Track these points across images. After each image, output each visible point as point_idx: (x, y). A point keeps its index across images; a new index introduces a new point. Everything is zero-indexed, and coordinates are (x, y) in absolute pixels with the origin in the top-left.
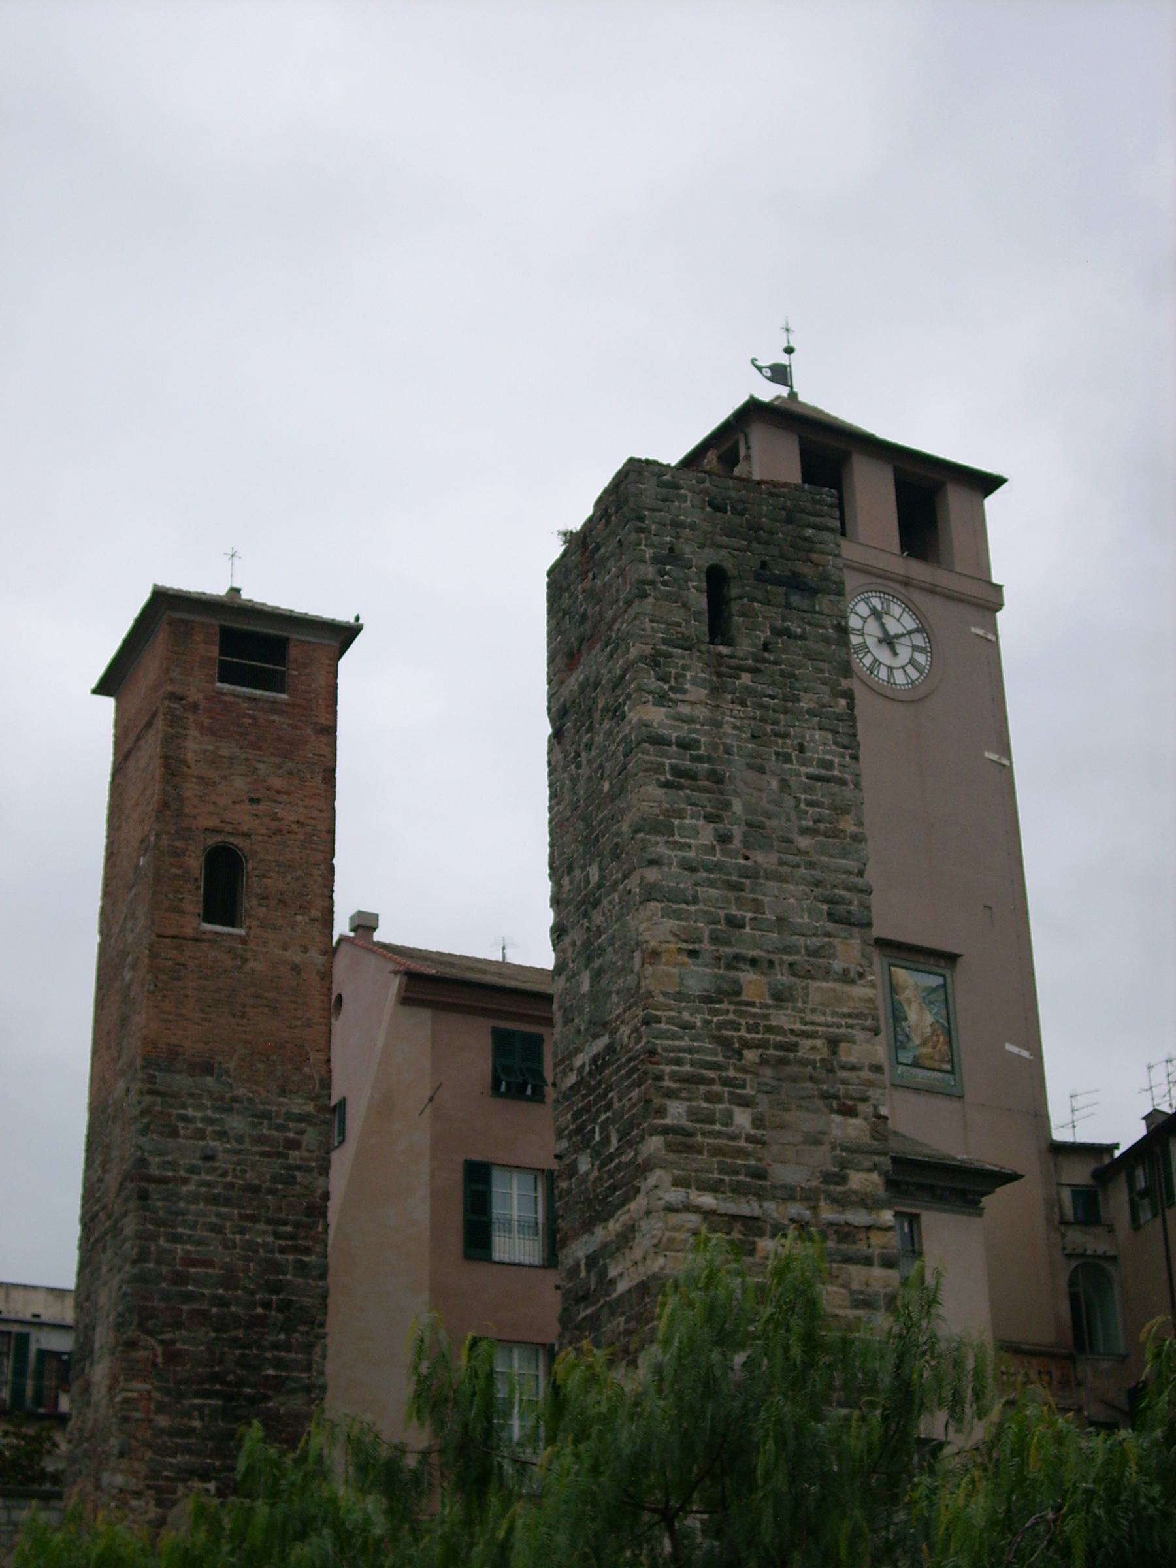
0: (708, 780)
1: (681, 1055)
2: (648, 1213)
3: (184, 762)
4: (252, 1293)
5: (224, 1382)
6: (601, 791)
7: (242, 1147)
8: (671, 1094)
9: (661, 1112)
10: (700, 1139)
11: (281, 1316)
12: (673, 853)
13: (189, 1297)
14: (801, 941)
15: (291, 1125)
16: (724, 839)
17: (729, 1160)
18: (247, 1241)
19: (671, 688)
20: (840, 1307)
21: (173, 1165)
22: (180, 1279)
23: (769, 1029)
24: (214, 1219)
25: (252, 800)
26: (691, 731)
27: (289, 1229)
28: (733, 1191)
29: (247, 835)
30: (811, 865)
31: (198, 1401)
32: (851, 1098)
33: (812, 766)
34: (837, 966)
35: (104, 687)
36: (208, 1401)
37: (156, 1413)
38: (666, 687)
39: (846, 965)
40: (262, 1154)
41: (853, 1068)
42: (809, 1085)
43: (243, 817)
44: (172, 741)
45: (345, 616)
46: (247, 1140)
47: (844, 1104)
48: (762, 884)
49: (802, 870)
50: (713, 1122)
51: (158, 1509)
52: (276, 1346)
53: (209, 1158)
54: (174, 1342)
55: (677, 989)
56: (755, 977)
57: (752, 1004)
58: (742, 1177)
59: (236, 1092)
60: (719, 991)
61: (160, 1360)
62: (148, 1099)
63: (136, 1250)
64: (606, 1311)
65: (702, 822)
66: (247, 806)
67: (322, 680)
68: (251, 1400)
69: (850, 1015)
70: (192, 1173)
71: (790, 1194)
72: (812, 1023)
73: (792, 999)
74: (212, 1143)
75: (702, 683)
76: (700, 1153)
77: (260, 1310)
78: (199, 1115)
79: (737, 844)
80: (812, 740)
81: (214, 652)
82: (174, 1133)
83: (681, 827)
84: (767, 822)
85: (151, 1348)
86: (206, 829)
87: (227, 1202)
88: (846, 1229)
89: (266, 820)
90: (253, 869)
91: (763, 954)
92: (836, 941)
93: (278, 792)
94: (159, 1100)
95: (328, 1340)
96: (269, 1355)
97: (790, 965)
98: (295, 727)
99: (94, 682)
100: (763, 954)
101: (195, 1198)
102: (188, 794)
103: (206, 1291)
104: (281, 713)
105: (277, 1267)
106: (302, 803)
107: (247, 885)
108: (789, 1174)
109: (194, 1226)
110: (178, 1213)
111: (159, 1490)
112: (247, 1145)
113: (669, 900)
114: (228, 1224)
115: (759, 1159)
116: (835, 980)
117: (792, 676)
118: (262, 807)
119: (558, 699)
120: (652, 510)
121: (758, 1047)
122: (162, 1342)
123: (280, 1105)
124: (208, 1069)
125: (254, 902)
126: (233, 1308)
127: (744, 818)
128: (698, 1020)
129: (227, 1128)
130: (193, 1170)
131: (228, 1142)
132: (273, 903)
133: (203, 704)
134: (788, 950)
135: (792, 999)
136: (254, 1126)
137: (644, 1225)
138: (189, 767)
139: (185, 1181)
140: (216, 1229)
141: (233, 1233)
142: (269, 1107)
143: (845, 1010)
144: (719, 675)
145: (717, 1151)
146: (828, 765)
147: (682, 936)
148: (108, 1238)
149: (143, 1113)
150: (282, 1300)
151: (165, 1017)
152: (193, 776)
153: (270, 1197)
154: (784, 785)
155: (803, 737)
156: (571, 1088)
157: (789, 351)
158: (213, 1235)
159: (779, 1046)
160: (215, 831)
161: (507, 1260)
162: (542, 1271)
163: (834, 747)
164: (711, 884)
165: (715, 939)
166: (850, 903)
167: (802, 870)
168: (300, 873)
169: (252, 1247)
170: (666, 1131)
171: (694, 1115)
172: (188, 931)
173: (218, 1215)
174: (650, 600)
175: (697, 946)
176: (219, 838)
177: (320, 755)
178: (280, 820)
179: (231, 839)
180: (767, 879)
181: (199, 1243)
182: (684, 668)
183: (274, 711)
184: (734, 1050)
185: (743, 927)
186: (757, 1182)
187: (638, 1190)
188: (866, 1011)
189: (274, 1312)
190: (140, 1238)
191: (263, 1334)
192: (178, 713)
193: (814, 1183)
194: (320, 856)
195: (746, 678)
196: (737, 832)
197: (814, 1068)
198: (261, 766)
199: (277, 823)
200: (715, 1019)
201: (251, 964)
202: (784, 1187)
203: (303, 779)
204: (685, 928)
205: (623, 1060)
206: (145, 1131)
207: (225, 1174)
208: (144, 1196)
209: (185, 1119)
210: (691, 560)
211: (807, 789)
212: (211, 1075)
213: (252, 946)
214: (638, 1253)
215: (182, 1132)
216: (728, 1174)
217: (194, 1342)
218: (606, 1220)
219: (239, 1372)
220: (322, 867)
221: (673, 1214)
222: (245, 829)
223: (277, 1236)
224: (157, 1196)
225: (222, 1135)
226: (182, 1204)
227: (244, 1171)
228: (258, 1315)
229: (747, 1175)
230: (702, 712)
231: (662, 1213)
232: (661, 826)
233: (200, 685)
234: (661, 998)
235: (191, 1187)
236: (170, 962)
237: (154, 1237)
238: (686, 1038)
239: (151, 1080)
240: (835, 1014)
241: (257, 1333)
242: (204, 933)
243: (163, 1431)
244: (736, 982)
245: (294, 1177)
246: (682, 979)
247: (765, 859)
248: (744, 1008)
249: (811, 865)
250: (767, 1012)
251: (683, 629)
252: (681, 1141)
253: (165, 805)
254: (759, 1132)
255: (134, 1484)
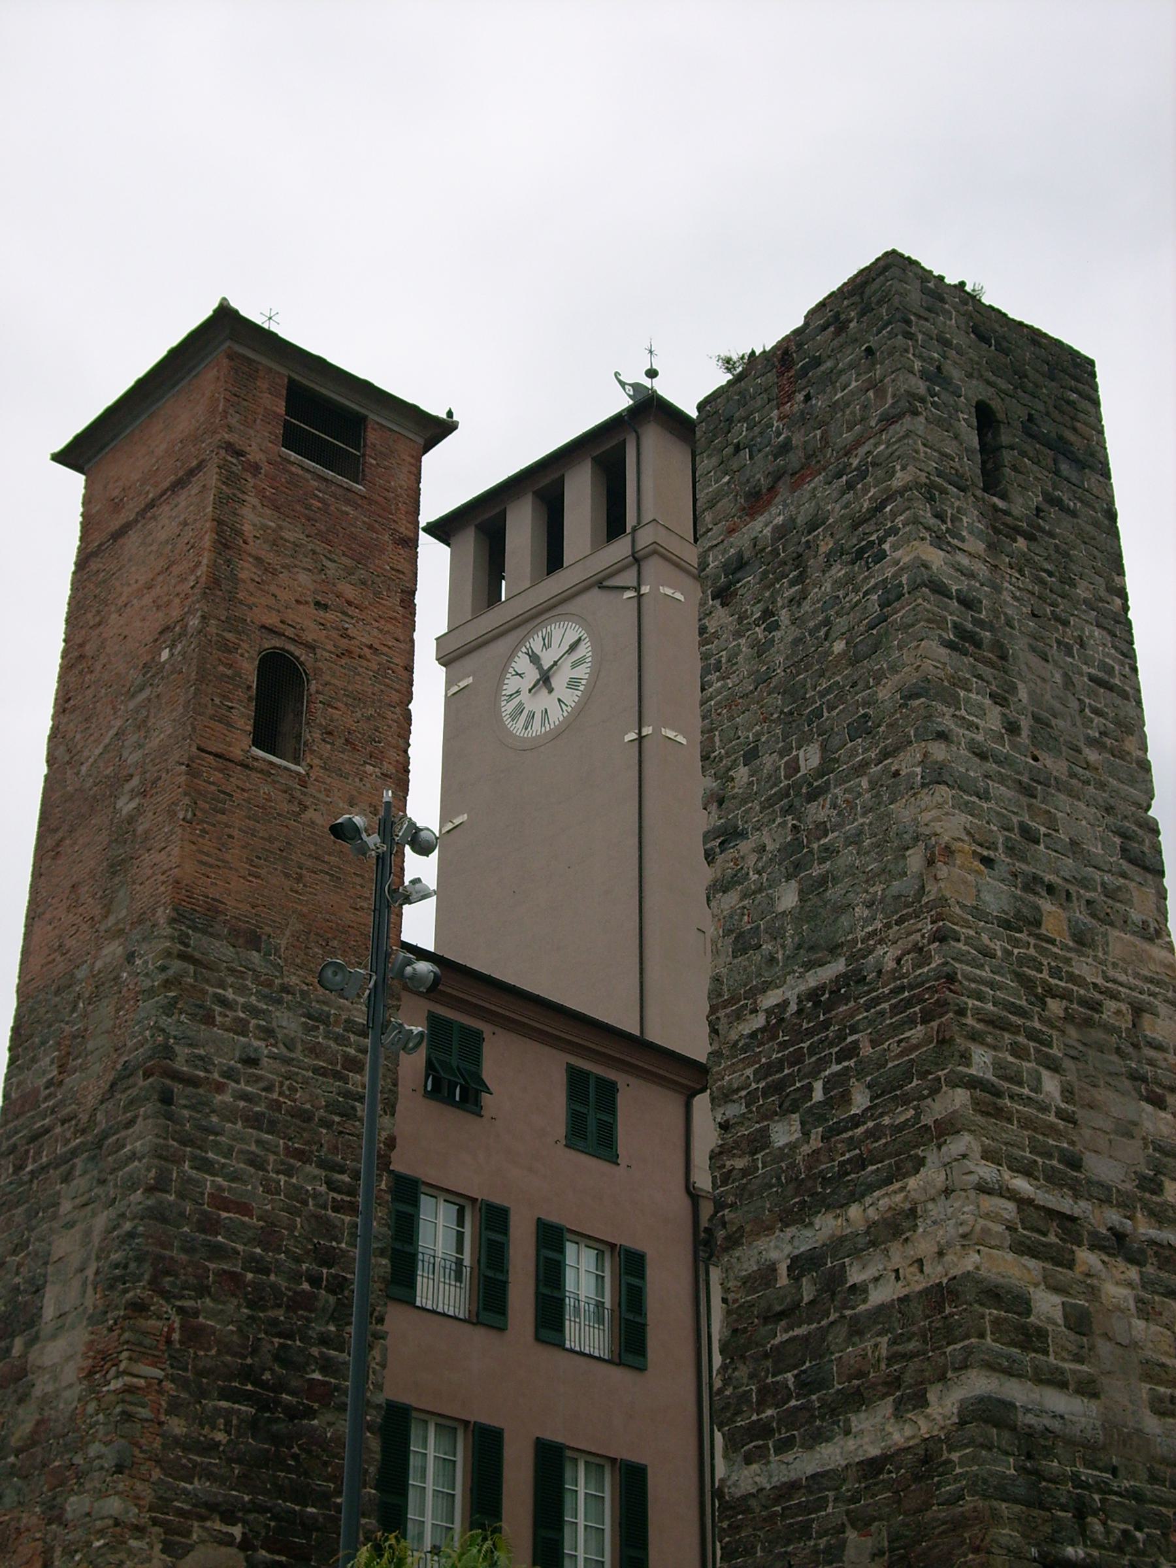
0: (992, 652)
1: (983, 988)
2: (947, 1192)
3: (239, 533)
4: (298, 1260)
5: (257, 1382)
6: (828, 653)
7: (293, 1055)
8: (974, 1037)
9: (965, 1058)
10: (1007, 1101)
11: (332, 1299)
12: (961, 731)
13: (217, 1252)
14: (1097, 876)
15: (353, 1038)
16: (1013, 728)
17: (1040, 1137)
18: (294, 1185)
19: (948, 530)
20: (1166, 1353)
21: (205, 1062)
22: (208, 1225)
23: (1072, 978)
24: (253, 1148)
25: (317, 604)
26: (970, 587)
27: (345, 1178)
28: (1048, 1179)
29: (311, 647)
30: (1102, 786)
31: (224, 1404)
32: (1160, 1085)
33: (1093, 667)
34: (1135, 916)
35: (73, 455)
36: (236, 1406)
37: (167, 1413)
38: (944, 527)
39: (1144, 918)
40: (316, 1070)
41: (1159, 1048)
42: (1115, 1058)
43: (307, 621)
44: (227, 502)
45: (438, 410)
46: (299, 1047)
47: (1153, 1091)
48: (1053, 795)
49: (1091, 789)
50: (1020, 1084)
51: (164, 1556)
52: (324, 1340)
53: (251, 1061)
54: (196, 1314)
55: (974, 903)
56: (1054, 908)
57: (1052, 942)
58: (1055, 1163)
59: (286, 980)
60: (1018, 915)
61: (176, 1336)
62: (177, 965)
63: (152, 1174)
64: (843, 1331)
65: (988, 701)
66: (311, 609)
67: (402, 479)
68: (293, 1414)
69: (1151, 980)
70: (228, 1078)
71: (1105, 1196)
72: (1115, 981)
73: (1092, 945)
74: (256, 1043)
75: (979, 535)
76: (1010, 1121)
77: (306, 1286)
78: (242, 1000)
79: (1024, 737)
80: (1091, 636)
81: (281, 408)
82: (209, 1020)
83: (967, 701)
84: (1054, 722)
85: (165, 1320)
86: (263, 627)
87: (272, 1128)
88: (1167, 1253)
89: (334, 634)
90: (318, 692)
91: (1060, 881)
92: (1132, 885)
93: (350, 603)
94: (191, 968)
95: (389, 1342)
96: (315, 1351)
97: (1088, 902)
98: (371, 528)
99: (58, 447)
100: (1060, 881)
101: (231, 1115)
102: (244, 575)
103: (240, 1247)
104: (356, 506)
105: (330, 1229)
106: (377, 624)
107: (309, 711)
108: (1103, 1168)
109: (228, 1154)
110: (209, 1130)
111: (169, 1529)
112: (297, 1054)
113: (960, 788)
114: (272, 1158)
115: (1072, 1143)
116: (1134, 933)
117: (1066, 555)
118: (330, 616)
119: (725, 551)
120: (920, 317)
121: (1062, 998)
122: (181, 1310)
123: (340, 1008)
124: (254, 941)
125: (317, 735)
126: (273, 1277)
127: (1031, 709)
128: (997, 947)
129: (274, 1024)
130: (230, 1074)
131: (275, 1045)
132: (340, 742)
133: (265, 467)
134: (1085, 883)
135: (1092, 945)
136: (308, 1029)
137: (935, 1210)
138: (245, 542)
139: (220, 1088)
140: (256, 1163)
141: (278, 1172)
142: (326, 1009)
143: (1146, 972)
144: (997, 531)
145: (1027, 1123)
146: (1110, 671)
147: (977, 836)
148: (79, 1162)
149: (167, 984)
150: (336, 1276)
151: (205, 858)
152: (250, 555)
153: (324, 1131)
154: (1068, 683)
155: (1083, 630)
156: (753, 1035)
157: (652, 374)
158: (252, 1170)
159: (1083, 1002)
160: (271, 630)
161: (429, 1307)
162: (467, 1328)
163: (1113, 651)
164: (1002, 780)
165: (1010, 850)
166: (1142, 842)
167: (1091, 789)
168: (371, 711)
169: (298, 1195)
170: (973, 1083)
171: (999, 1067)
172: (237, 753)
173: (259, 1142)
174: (922, 419)
175: (992, 854)
176: (277, 642)
177: (398, 571)
178: (351, 638)
179: (291, 647)
180: (1059, 790)
181: (234, 1177)
182: (959, 510)
183: (348, 502)
184: (1036, 996)
185: (1037, 842)
186: (1068, 1170)
187: (921, 1162)
188: (1167, 979)
189: (323, 1292)
190: (160, 1157)
191: (308, 1319)
192: (234, 469)
193: (1129, 1186)
194: (395, 697)
195: (1021, 543)
196: (1025, 723)
197: (1120, 1037)
198: (328, 564)
199: (346, 641)
200: (1016, 951)
201: (310, 814)
202: (1101, 1184)
203: (378, 594)
204: (979, 828)
205: (886, 990)
206: (169, 1008)
207: (269, 1089)
208: (167, 1098)
209: (223, 1002)
210: (959, 388)
211: (1092, 694)
212: (258, 951)
213: (311, 790)
214: (924, 1247)
215: (218, 1019)
216: (1040, 1154)
217: (222, 1317)
218: (844, 1206)
219: (276, 1368)
220: (398, 710)
221: (986, 1197)
222: (309, 637)
223: (331, 1186)
224: (183, 1102)
225: (268, 1033)
226: (215, 1119)
227: (292, 1089)
228: (303, 1291)
229: (1059, 1161)
230: (981, 569)
231: (972, 1194)
232: (946, 691)
233: (262, 443)
234: (958, 910)
235: (227, 1098)
236: (213, 788)
237: (178, 1161)
238: (987, 968)
239: (183, 940)
240: (1137, 975)
241: (301, 1318)
242: (256, 759)
243: (177, 1441)
244: (1037, 909)
245: (354, 1108)
246: (979, 891)
247: (1055, 765)
248: (1044, 945)
249: (1102, 786)
250: (1069, 955)
251: (956, 465)
252: (990, 1099)
253: (215, 582)
254: (1071, 1108)
255: (133, 1515)
